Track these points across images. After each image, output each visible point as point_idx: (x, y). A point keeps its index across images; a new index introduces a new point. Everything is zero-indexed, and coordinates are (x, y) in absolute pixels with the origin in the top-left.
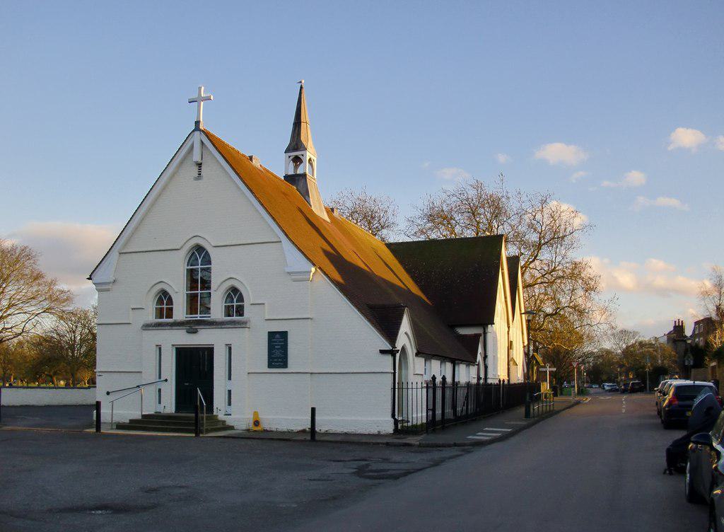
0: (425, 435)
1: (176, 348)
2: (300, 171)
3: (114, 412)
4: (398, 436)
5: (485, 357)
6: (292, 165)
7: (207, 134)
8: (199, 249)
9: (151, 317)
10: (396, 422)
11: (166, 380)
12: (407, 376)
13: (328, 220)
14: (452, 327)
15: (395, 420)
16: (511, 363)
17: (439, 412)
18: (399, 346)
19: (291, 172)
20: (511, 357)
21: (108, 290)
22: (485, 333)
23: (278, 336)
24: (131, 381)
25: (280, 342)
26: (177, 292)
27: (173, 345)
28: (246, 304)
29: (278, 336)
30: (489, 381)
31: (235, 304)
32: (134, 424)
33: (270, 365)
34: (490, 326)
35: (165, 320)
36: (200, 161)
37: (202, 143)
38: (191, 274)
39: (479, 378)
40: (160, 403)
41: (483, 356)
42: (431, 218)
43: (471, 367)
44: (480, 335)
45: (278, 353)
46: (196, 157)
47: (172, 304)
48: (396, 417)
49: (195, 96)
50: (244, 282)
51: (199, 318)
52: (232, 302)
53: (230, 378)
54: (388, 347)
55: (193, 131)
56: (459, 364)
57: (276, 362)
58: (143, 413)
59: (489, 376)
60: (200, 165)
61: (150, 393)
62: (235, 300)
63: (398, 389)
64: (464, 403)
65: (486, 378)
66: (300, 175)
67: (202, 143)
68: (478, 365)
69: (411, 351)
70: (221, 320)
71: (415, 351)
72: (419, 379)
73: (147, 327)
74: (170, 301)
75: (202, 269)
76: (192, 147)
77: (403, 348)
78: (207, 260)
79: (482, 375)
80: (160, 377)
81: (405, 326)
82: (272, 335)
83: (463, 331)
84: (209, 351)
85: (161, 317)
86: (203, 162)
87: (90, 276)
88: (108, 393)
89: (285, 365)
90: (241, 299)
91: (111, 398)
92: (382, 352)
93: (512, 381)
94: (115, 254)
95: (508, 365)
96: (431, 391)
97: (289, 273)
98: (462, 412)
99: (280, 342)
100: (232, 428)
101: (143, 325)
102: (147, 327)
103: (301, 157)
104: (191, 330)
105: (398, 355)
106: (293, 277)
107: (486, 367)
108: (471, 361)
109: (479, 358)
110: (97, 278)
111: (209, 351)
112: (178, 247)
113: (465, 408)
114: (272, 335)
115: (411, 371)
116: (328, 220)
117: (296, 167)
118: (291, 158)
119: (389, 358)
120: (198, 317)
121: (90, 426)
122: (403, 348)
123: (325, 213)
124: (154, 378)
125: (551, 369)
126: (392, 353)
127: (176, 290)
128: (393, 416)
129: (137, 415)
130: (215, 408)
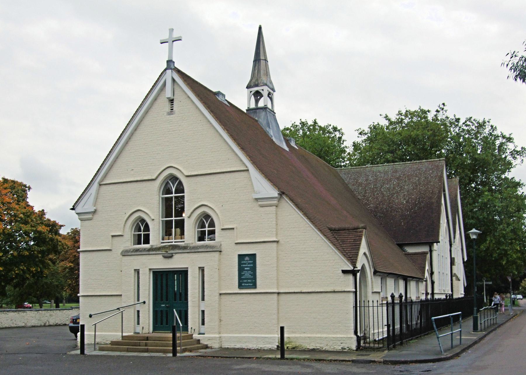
0: (387, 351)
1: (153, 272)
2: (261, 104)
3: (94, 333)
4: (361, 353)
5: (432, 273)
6: (253, 99)
7: (179, 72)
8: (174, 178)
9: (128, 243)
10: (359, 339)
11: (144, 302)
12: (366, 296)
13: (287, 149)
14: (401, 246)
15: (358, 336)
16: (454, 278)
17: (397, 326)
18: (359, 267)
19: (253, 106)
20: (454, 272)
21: (90, 219)
22: (431, 251)
23: (247, 258)
24: (115, 303)
25: (249, 264)
26: (153, 220)
27: (150, 269)
28: (217, 229)
29: (247, 258)
30: (436, 297)
31: (207, 229)
32: (115, 345)
33: (240, 286)
34: (435, 244)
35: (143, 246)
36: (172, 97)
37: (174, 80)
38: (167, 202)
39: (427, 294)
40: (138, 324)
41: (430, 272)
42: (334, 127)
43: (420, 284)
44: (425, 253)
45: (247, 274)
46: (168, 93)
47: (149, 231)
48: (359, 334)
49: (166, 37)
50: (215, 209)
51: (174, 243)
52: (205, 227)
53: (203, 299)
54: (351, 268)
55: (165, 70)
56: (410, 281)
57: (245, 283)
58: (124, 334)
59: (436, 291)
60: (172, 101)
61: (130, 315)
62: (207, 226)
63: (360, 307)
64: (418, 317)
65: (433, 294)
66: (261, 108)
67: (174, 80)
68: (426, 281)
69: (369, 272)
70: (194, 245)
71: (372, 270)
72: (376, 297)
73: (125, 253)
74: (147, 228)
75: (176, 197)
76: (165, 84)
77: (363, 267)
78: (180, 189)
79: (430, 291)
80: (138, 300)
81: (364, 248)
82: (241, 257)
83: (411, 250)
84: (183, 273)
85: (139, 243)
86: (175, 97)
87: (73, 206)
88: (91, 316)
89: (254, 286)
90: (212, 224)
91: (94, 320)
92: (344, 272)
93: (455, 296)
94: (96, 185)
95: (452, 280)
96: (390, 309)
97: (257, 200)
98: (417, 324)
99: (249, 264)
100: (206, 347)
101: (122, 252)
102: (125, 253)
103: (261, 91)
104: (166, 255)
105: (358, 274)
106: (260, 203)
107: (433, 283)
108: (419, 280)
109: (427, 275)
110: (79, 209)
111: (183, 273)
112: (154, 177)
113: (419, 321)
114: (241, 257)
115: (370, 291)
116: (287, 149)
117: (257, 101)
118: (253, 93)
119: (351, 277)
120: (173, 241)
121: (75, 347)
122: (363, 267)
123: (284, 144)
124: (132, 300)
125: (488, 283)
126: (354, 273)
127: (153, 218)
128: (356, 333)
129: (117, 336)
130: (189, 327)
